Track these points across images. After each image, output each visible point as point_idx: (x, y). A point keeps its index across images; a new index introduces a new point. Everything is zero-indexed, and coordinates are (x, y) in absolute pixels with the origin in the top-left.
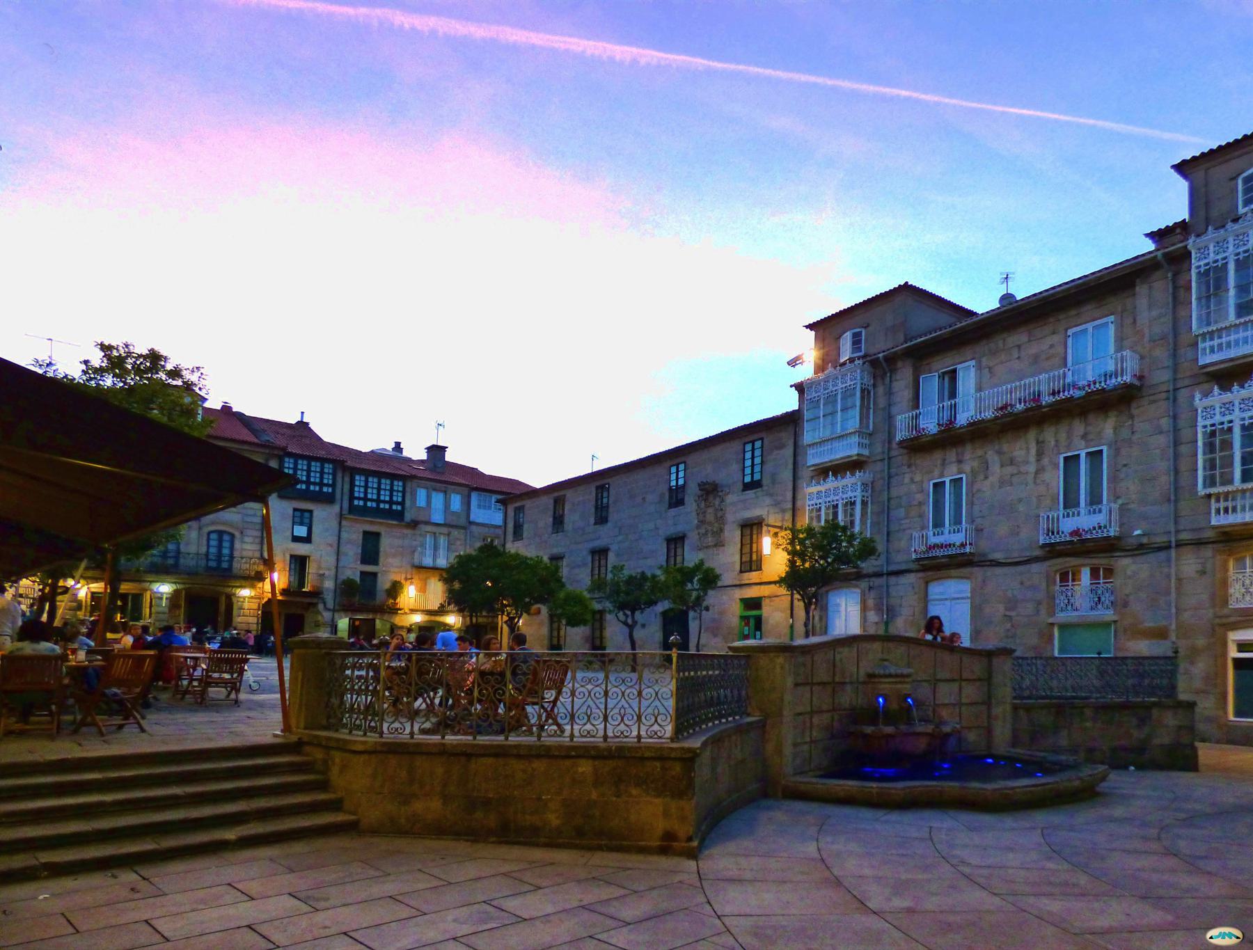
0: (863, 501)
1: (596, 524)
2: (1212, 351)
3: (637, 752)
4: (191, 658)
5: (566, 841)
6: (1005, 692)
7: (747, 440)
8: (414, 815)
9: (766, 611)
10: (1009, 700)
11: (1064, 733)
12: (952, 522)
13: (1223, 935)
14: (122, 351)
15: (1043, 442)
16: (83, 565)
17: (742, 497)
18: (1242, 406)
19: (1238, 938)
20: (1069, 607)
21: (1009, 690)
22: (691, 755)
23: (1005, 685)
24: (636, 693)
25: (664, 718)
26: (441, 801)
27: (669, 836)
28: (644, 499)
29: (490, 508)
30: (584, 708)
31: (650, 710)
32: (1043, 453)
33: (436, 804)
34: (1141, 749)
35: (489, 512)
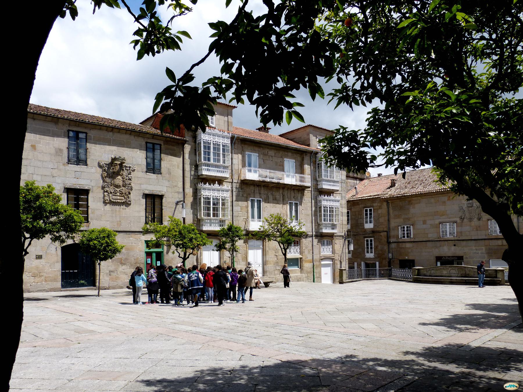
4: (73, 131)
5: (235, 308)
12: (237, 196)
13: (510, 386)
14: (476, 75)
19: (517, 387)
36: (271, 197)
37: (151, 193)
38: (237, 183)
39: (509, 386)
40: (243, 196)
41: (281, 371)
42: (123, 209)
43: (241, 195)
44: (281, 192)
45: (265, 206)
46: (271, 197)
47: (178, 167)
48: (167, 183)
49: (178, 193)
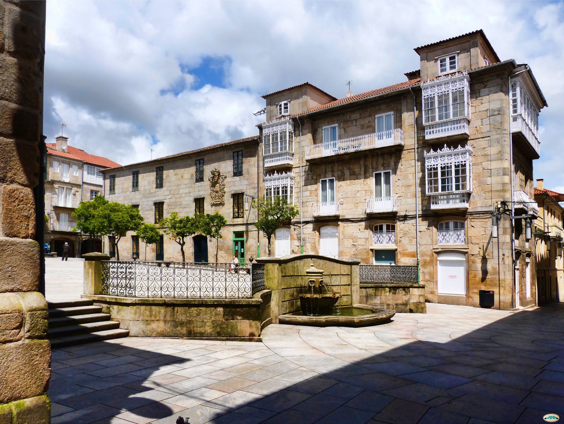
0: (291, 186)
1: (157, 188)
3: (240, 303)
6: (357, 280)
7: (235, 150)
8: (152, 329)
10: (358, 283)
11: (379, 297)
13: (551, 418)
15: (367, 166)
17: (233, 180)
19: (557, 419)
20: (378, 242)
21: (358, 279)
23: (357, 277)
24: (224, 279)
25: (197, 289)
26: (164, 323)
27: (252, 335)
28: (182, 177)
29: (94, 174)
30: (243, 286)
31: (178, 286)
32: (367, 171)
33: (162, 324)
34: (406, 304)
35: (92, 176)
36: (347, 173)
37: (235, 193)
38: (306, 166)
40: (312, 178)
42: (221, 208)
43: (310, 178)
44: (362, 163)
45: (339, 186)
46: (347, 173)
47: (254, 166)
48: (246, 182)
49: (254, 188)
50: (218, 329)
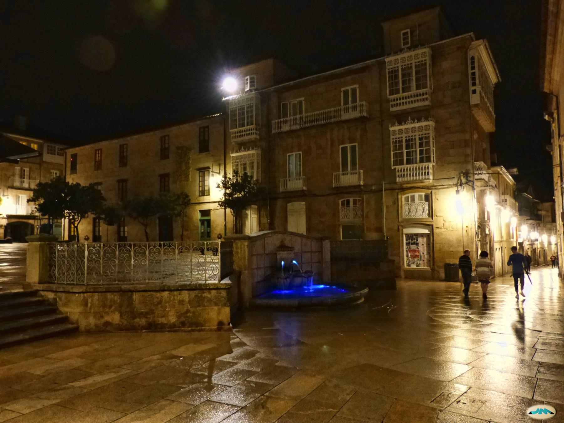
2: (395, 106)
9: (213, 216)
13: (540, 411)
16: (224, 99)
18: (406, 131)
19: (552, 413)
22: (229, 287)
25: (216, 271)
39: (536, 412)
41: (144, 287)
50: (183, 319)
